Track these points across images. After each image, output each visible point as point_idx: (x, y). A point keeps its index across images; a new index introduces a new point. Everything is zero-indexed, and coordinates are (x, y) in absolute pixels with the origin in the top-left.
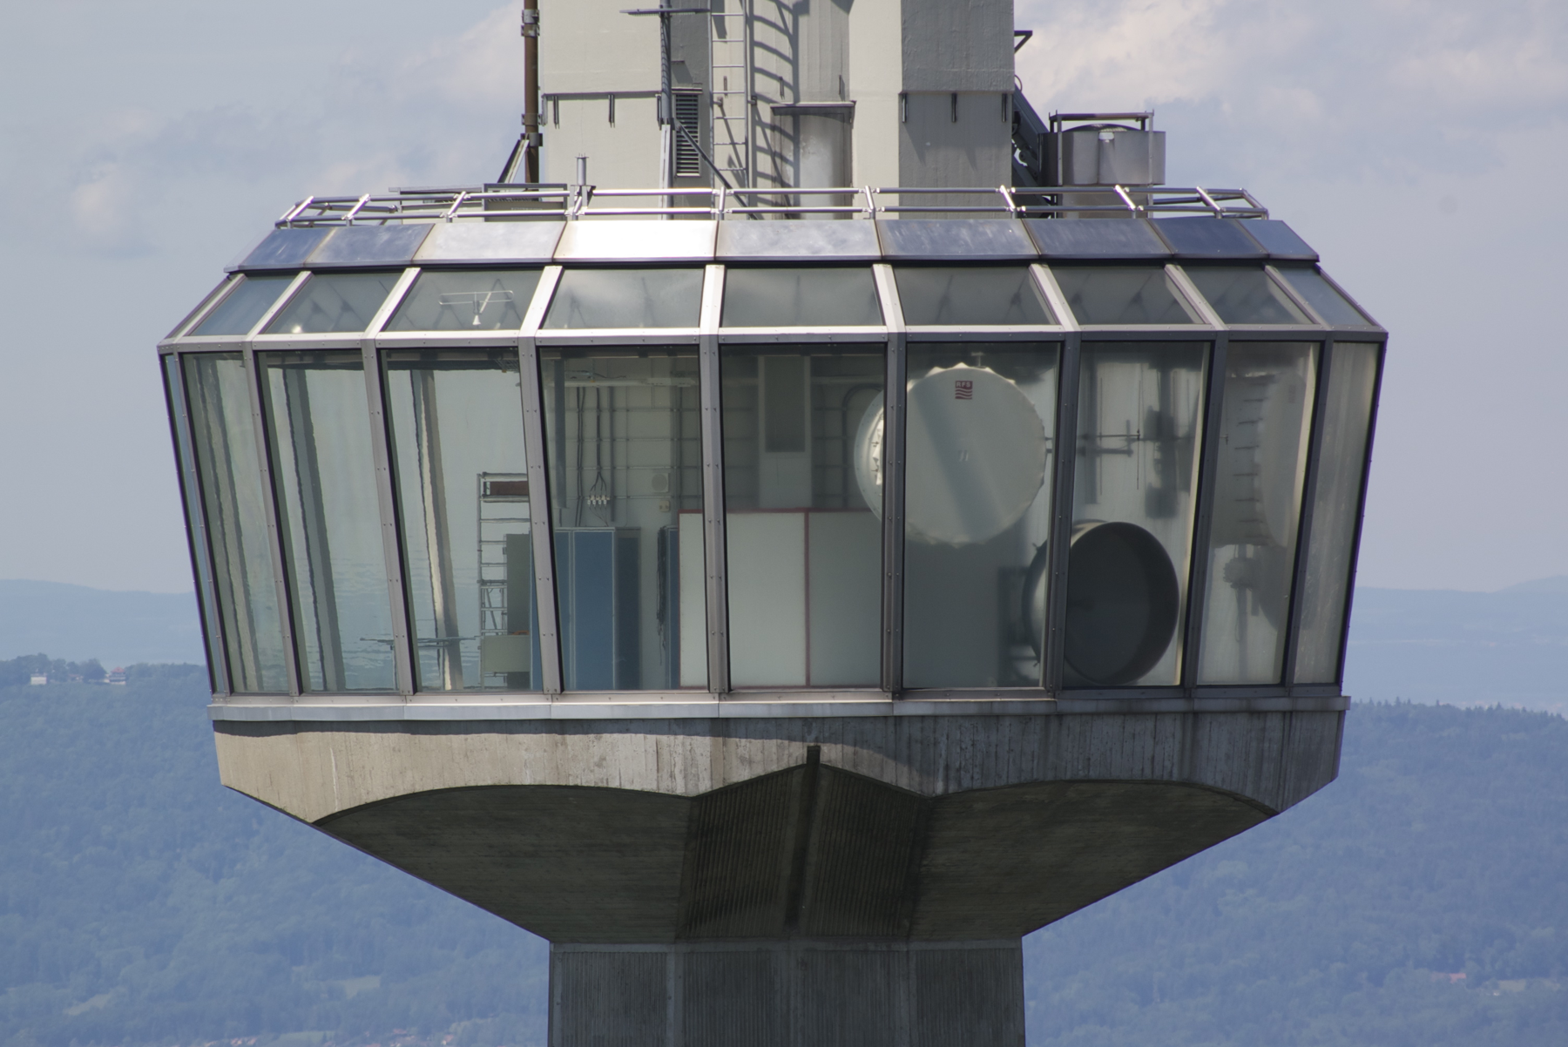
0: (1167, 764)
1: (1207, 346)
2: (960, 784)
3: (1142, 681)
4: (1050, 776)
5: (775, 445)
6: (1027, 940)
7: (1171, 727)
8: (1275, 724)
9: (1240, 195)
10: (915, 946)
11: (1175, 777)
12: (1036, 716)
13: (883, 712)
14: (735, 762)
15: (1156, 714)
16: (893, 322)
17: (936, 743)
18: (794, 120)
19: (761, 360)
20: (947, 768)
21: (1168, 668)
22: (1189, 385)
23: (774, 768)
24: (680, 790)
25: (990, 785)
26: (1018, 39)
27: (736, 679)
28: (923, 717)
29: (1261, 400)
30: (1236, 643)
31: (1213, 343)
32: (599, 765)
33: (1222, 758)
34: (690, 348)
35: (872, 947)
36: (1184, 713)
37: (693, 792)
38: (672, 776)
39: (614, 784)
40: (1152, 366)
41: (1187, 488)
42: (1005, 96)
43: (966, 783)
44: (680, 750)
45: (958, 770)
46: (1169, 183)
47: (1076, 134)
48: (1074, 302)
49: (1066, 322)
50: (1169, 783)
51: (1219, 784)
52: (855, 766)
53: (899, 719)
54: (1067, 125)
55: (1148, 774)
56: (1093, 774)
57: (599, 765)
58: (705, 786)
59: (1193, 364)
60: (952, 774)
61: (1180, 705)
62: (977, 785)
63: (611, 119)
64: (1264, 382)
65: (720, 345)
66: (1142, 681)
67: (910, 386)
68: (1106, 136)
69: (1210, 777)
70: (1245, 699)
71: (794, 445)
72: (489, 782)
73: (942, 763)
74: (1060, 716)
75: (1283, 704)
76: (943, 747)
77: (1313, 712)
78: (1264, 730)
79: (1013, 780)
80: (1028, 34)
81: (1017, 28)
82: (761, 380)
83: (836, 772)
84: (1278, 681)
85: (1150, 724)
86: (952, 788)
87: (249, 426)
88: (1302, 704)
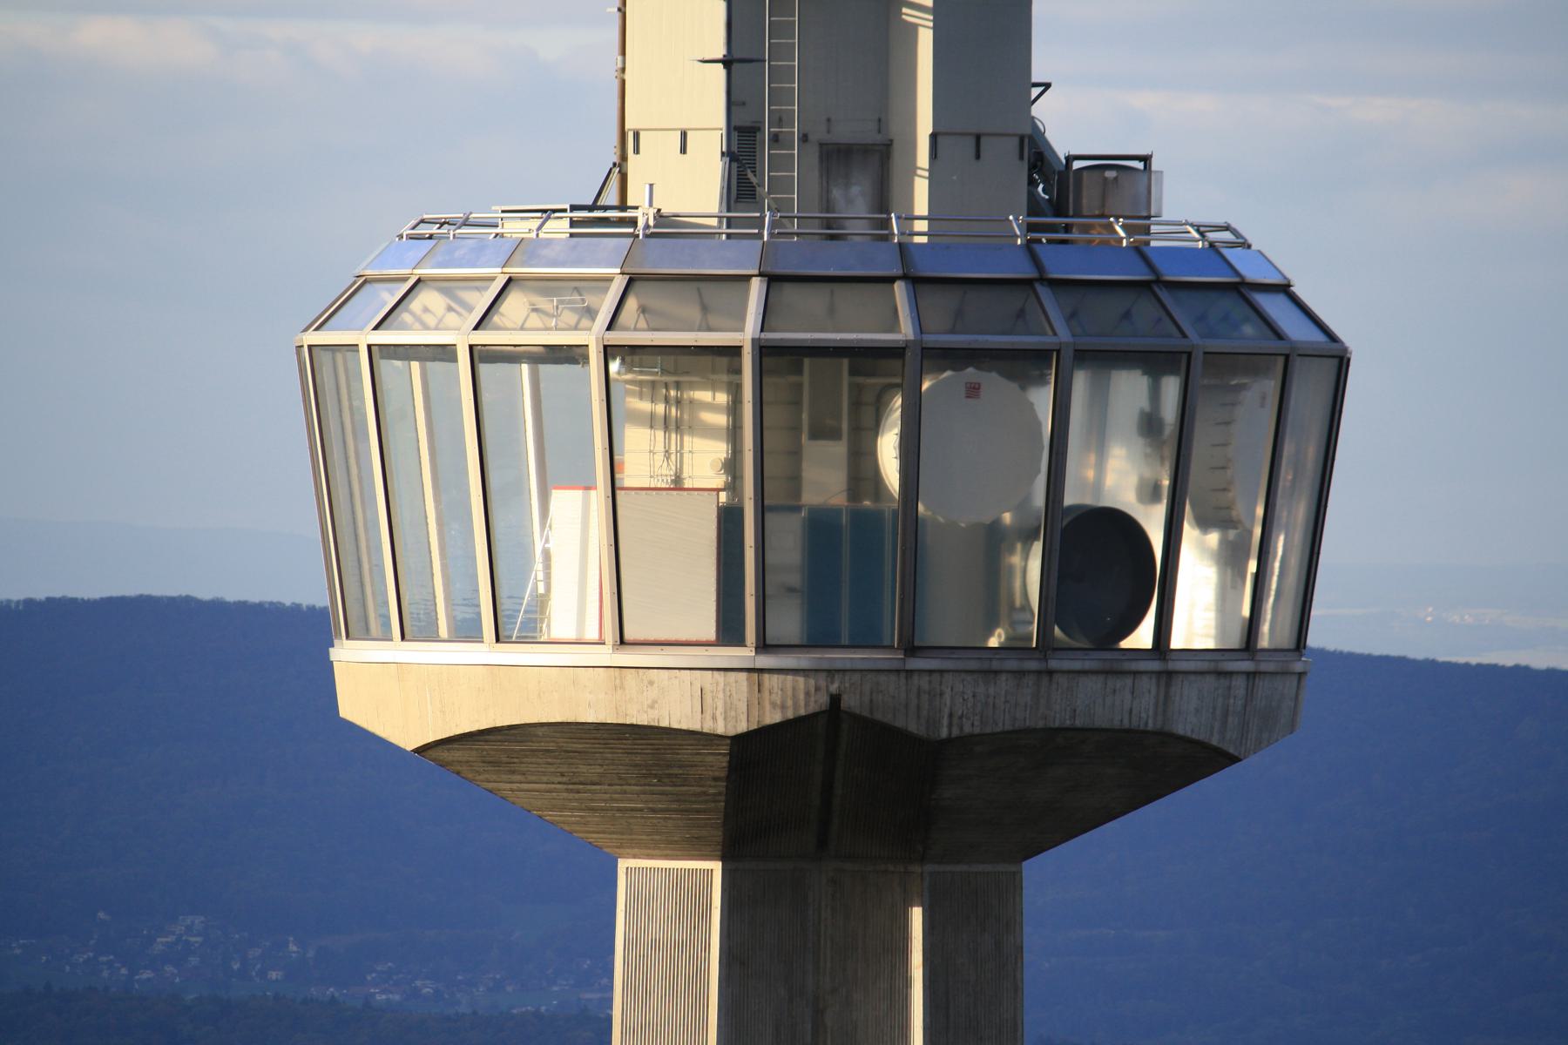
0: (1144, 715)
1: (1185, 357)
2: (961, 729)
3: (1126, 644)
4: (1041, 724)
5: (818, 434)
6: (1033, 869)
7: (1147, 684)
8: (1239, 684)
9: (1227, 228)
10: (929, 868)
11: (1150, 727)
12: (1029, 672)
13: (896, 665)
14: (768, 707)
15: (1136, 673)
16: (906, 330)
17: (941, 694)
18: (837, 158)
19: (807, 361)
20: (951, 715)
21: (1142, 637)
22: (1171, 387)
23: (802, 712)
24: (720, 730)
25: (988, 730)
26: (1035, 92)
27: (628, 636)
28: (931, 672)
29: (1233, 404)
30: (1199, 611)
31: (1189, 354)
32: (652, 707)
33: (1191, 715)
34: (735, 351)
35: (891, 868)
36: (1039, 672)
37: (732, 733)
38: (714, 718)
39: (664, 724)
40: (1145, 373)
41: (1039, 471)
42: (1022, 139)
43: (967, 729)
44: (721, 695)
45: (961, 718)
46: (1165, 217)
47: (1085, 173)
48: (1071, 317)
49: (1064, 334)
50: (1145, 732)
51: (1189, 734)
52: (871, 711)
53: (910, 672)
54: (1077, 165)
55: (1126, 724)
56: (1078, 723)
57: (652, 707)
58: (742, 727)
59: (1173, 371)
60: (955, 720)
61: (1155, 666)
62: (977, 730)
63: (978, 157)
64: (1241, 387)
65: (761, 348)
66: (1126, 644)
67: (926, 386)
68: (1110, 174)
69: (1180, 729)
70: (1208, 663)
71: (834, 435)
72: (559, 720)
73: (946, 711)
74: (1051, 673)
75: (1247, 666)
76: (947, 697)
77: (1195, 673)
78: (1229, 688)
79: (1008, 727)
80: (1047, 86)
81: (1034, 79)
82: (806, 379)
83: (856, 718)
84: (1292, 646)
85: (1129, 681)
86: (956, 732)
87: (1281, 484)
88: (1264, 667)
